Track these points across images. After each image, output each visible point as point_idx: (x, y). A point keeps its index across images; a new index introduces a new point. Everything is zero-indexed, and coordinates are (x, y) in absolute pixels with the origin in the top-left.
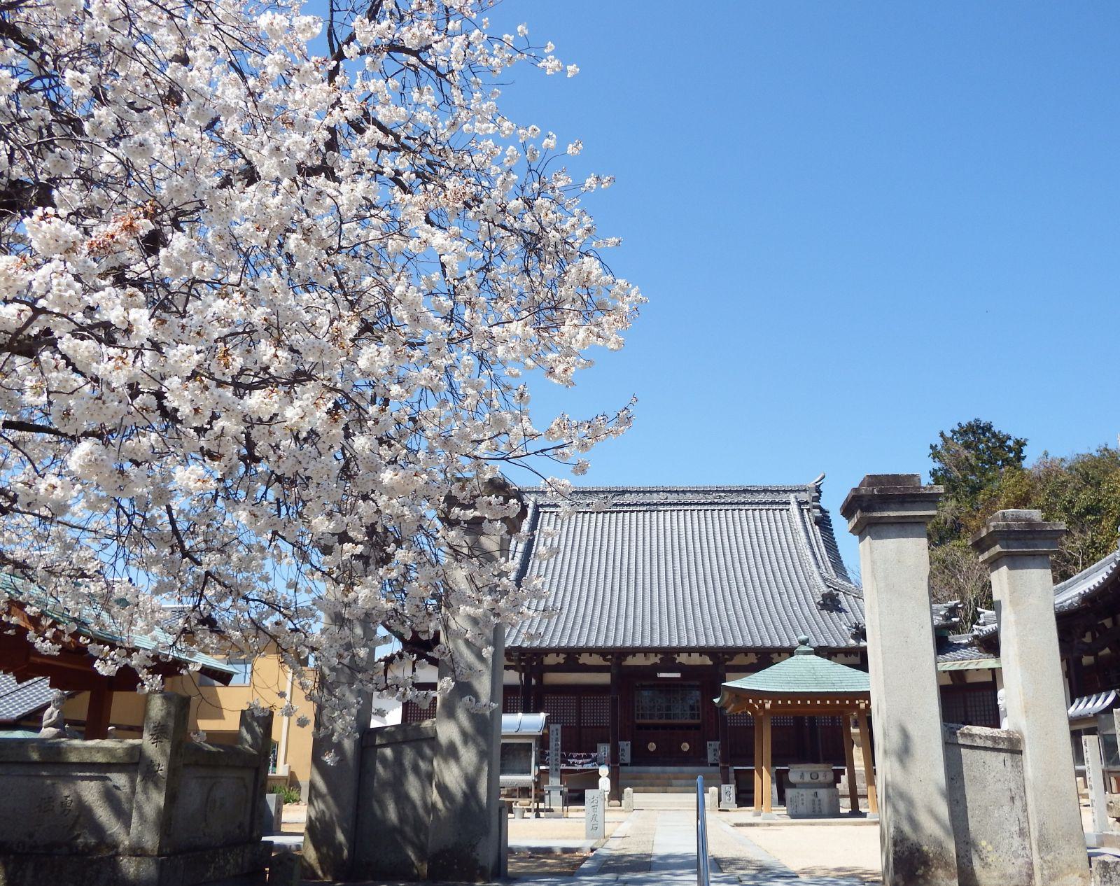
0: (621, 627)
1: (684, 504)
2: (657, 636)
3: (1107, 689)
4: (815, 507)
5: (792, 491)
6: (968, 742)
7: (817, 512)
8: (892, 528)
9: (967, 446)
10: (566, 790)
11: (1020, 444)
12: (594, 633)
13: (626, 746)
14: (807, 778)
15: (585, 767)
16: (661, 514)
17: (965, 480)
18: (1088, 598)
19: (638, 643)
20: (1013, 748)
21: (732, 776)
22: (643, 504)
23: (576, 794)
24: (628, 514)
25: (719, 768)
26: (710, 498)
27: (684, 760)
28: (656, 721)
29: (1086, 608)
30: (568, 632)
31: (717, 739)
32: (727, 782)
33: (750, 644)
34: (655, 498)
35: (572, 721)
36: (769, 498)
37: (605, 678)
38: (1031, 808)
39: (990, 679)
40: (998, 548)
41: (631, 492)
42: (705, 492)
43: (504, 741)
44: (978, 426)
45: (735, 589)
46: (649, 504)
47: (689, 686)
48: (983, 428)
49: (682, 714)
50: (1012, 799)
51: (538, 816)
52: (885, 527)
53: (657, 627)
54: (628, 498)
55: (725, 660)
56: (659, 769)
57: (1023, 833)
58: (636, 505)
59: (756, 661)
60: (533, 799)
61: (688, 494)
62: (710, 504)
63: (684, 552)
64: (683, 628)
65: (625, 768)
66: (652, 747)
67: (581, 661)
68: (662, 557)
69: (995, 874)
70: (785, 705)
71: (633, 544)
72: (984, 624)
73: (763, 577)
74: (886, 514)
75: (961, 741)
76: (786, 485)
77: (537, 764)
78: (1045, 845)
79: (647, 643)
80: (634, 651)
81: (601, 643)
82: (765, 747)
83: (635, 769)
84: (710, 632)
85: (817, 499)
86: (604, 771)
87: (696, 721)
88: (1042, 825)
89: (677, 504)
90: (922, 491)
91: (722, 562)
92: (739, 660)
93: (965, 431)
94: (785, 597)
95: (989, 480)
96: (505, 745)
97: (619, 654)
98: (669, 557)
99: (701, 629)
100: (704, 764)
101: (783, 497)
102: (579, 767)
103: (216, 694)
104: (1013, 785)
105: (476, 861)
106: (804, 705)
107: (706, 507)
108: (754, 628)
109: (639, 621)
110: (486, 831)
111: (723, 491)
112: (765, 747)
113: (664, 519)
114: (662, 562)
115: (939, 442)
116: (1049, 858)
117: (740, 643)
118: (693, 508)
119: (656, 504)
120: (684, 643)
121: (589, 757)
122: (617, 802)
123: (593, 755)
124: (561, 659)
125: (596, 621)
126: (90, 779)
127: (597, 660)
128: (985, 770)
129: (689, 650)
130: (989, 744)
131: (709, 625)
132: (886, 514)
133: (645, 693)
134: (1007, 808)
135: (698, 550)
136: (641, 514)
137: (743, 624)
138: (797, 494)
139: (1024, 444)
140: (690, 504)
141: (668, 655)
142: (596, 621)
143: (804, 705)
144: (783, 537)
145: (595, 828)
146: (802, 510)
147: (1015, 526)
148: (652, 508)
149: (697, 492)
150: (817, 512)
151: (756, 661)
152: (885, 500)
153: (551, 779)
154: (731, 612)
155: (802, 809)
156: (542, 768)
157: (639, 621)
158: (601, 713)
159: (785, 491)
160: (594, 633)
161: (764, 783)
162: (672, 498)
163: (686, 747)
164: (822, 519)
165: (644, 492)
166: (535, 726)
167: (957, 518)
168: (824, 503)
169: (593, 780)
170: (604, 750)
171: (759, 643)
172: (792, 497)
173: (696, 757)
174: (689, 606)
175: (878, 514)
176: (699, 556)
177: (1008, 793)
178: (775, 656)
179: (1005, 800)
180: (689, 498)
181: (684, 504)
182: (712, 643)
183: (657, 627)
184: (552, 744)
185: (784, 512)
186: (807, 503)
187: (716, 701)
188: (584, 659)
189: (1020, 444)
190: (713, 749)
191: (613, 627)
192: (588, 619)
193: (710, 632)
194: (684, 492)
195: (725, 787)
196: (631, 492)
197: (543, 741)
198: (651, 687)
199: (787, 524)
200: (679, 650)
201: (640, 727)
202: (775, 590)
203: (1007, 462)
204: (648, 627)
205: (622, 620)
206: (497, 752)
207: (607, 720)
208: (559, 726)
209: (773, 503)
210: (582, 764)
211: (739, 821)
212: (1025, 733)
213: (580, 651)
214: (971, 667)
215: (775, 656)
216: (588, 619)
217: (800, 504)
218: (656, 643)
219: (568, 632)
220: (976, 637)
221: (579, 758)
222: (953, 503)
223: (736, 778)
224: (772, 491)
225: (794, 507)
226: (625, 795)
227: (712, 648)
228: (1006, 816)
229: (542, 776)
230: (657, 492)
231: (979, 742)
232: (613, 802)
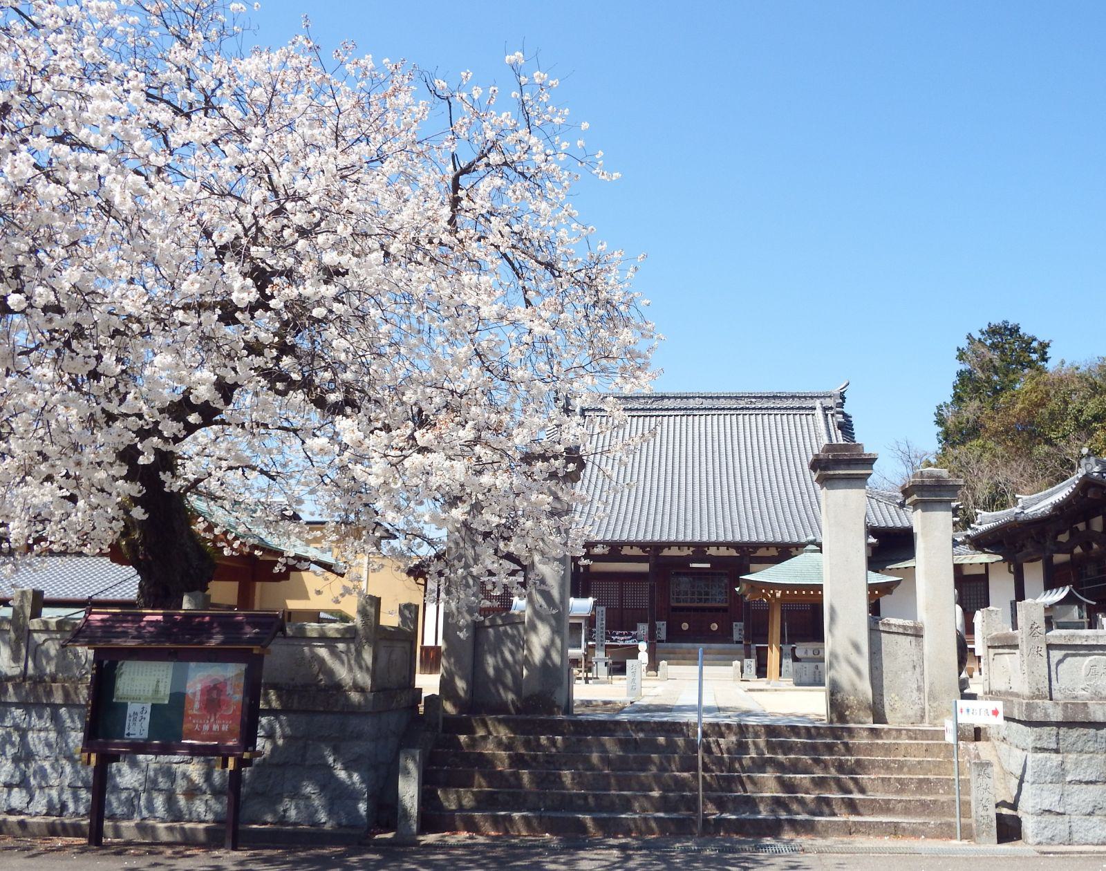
0: (659, 523)
1: (717, 409)
2: (689, 532)
3: (1064, 585)
4: (838, 413)
5: (818, 397)
7: (840, 418)
8: (842, 483)
9: (994, 347)
10: (611, 661)
11: (1044, 346)
12: (635, 529)
13: (662, 626)
14: (810, 654)
15: (627, 643)
17: (988, 380)
18: (1057, 507)
19: (673, 538)
20: (917, 633)
21: (754, 652)
22: (680, 409)
24: (666, 418)
26: (742, 404)
28: (682, 604)
30: (611, 527)
32: (749, 656)
33: (771, 539)
36: (796, 403)
37: (644, 567)
38: (926, 673)
40: (915, 497)
41: (669, 398)
42: (737, 398)
45: (761, 489)
46: (686, 409)
47: (719, 574)
48: (1010, 330)
50: (914, 667)
52: (836, 481)
53: (690, 523)
54: (667, 403)
56: (690, 645)
57: (919, 689)
60: (583, 669)
61: (722, 400)
62: (742, 409)
66: (685, 626)
67: (623, 553)
68: (697, 459)
70: (792, 594)
71: (671, 446)
73: (787, 478)
74: (837, 472)
75: (881, 628)
77: (586, 641)
78: (933, 697)
79: (681, 538)
80: (669, 545)
81: (640, 538)
82: (775, 630)
83: (670, 645)
85: (841, 405)
86: (643, 646)
87: (724, 605)
88: (932, 684)
89: (711, 409)
90: (863, 457)
92: (761, 552)
95: (1011, 381)
97: (658, 547)
98: (703, 458)
101: (809, 403)
102: (622, 643)
104: (915, 658)
106: (808, 594)
107: (738, 412)
108: (775, 524)
110: (560, 684)
111: (755, 397)
112: (775, 630)
113: (699, 423)
114: (697, 464)
115: (964, 344)
117: (762, 539)
118: (726, 412)
120: (713, 539)
121: (630, 634)
122: (654, 673)
123: (633, 633)
124: (606, 550)
125: (636, 517)
127: (637, 551)
128: (896, 649)
129: (718, 545)
130: (901, 630)
132: (837, 472)
136: (678, 418)
137: (767, 521)
138: (822, 400)
139: (1048, 345)
140: (724, 409)
141: (700, 549)
142: (636, 517)
143: (808, 594)
145: (632, 688)
146: (827, 415)
147: (927, 481)
148: (689, 412)
150: (840, 418)
152: (837, 463)
153: (596, 653)
154: (757, 510)
155: (805, 679)
156: (590, 643)
158: (641, 597)
159: (812, 398)
160: (635, 529)
161: (773, 656)
165: (682, 398)
166: (585, 609)
167: (978, 418)
169: (634, 653)
170: (643, 629)
171: (779, 539)
172: (817, 403)
173: (724, 636)
175: (831, 472)
177: (911, 663)
178: (793, 550)
180: (722, 403)
181: (717, 409)
182: (738, 538)
183: (690, 523)
184: (598, 623)
185: (810, 417)
186: (831, 408)
187: (737, 589)
188: (626, 551)
189: (1044, 346)
190: (738, 629)
192: (629, 516)
194: (718, 398)
195: (747, 661)
196: (669, 398)
197: (591, 621)
198: (685, 574)
199: (812, 428)
200: (709, 545)
201: (675, 609)
202: (797, 490)
203: (1031, 364)
204: (682, 523)
205: (659, 517)
206: (566, 631)
207: (646, 602)
208: (604, 608)
210: (624, 640)
213: (622, 544)
215: (793, 550)
216: (629, 516)
217: (825, 409)
218: (689, 539)
219: (611, 527)
220: (968, 536)
221: (621, 635)
222: (976, 403)
223: (758, 654)
224: (799, 398)
225: (819, 413)
227: (738, 543)
228: (910, 679)
229: (590, 650)
231: (894, 629)
232: (650, 673)
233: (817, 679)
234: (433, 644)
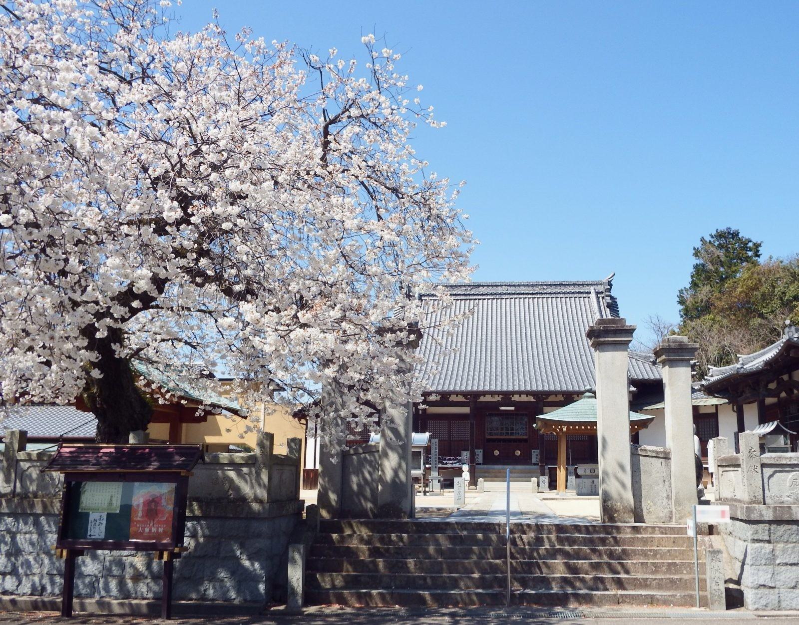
1: (519, 294)
2: (499, 383)
3: (773, 421)
4: (607, 296)
5: (592, 285)
6: (644, 454)
7: (608, 300)
8: (610, 347)
9: (720, 247)
10: (442, 479)
11: (757, 246)
12: (459, 382)
13: (479, 453)
14: (588, 472)
15: (454, 465)
16: (503, 301)
18: (768, 363)
19: (487, 389)
20: (666, 457)
21: (547, 471)
22: (491, 294)
23: (448, 482)
25: (538, 467)
26: (537, 290)
27: (516, 461)
29: (767, 370)
30: (442, 381)
31: (537, 448)
32: (543, 474)
33: (558, 389)
34: (500, 290)
35: (446, 437)
36: (577, 289)
37: (466, 410)
39: (714, 411)
40: (664, 357)
41: (483, 286)
43: (413, 450)
44: (729, 233)
46: (496, 294)
48: (732, 234)
49: (521, 433)
50: (664, 481)
51: (425, 494)
53: (499, 377)
54: (482, 290)
55: (544, 400)
58: (487, 294)
59: (563, 399)
60: (422, 485)
61: (522, 287)
63: (518, 327)
64: (516, 378)
65: (479, 466)
67: (450, 400)
69: (653, 516)
71: (485, 322)
72: (712, 376)
74: (606, 339)
75: (640, 453)
76: (588, 280)
77: (424, 464)
78: (678, 503)
79: (493, 388)
80: (484, 393)
81: (463, 389)
83: (485, 466)
84: (534, 381)
85: (609, 290)
86: (466, 468)
87: (525, 437)
88: (677, 493)
89: (514, 294)
90: (625, 328)
91: (543, 333)
92: (551, 398)
93: (720, 235)
94: (584, 358)
95: (733, 272)
96: (413, 452)
97: (476, 395)
99: (528, 379)
100: (530, 464)
101: (586, 289)
102: (450, 466)
103: (216, 419)
104: (665, 474)
105: (401, 509)
107: (534, 296)
108: (562, 378)
109: (488, 374)
110: (406, 496)
111: (546, 285)
113: (505, 304)
115: (698, 245)
116: (679, 509)
117: (552, 388)
118: (525, 296)
119: (500, 294)
120: (517, 389)
121: (456, 459)
122: (474, 487)
123: (458, 458)
125: (460, 374)
126: (230, 470)
127: (461, 398)
128: (651, 468)
129: (520, 393)
130: (654, 454)
131: (533, 376)
132: (606, 339)
133: (496, 418)
134: (661, 485)
135: (528, 325)
138: (595, 286)
139: (760, 245)
140: (523, 294)
141: (507, 396)
142: (460, 374)
144: (585, 316)
145: (459, 499)
146: (599, 298)
147: (673, 345)
148: (498, 297)
149: (528, 285)
150: (608, 300)
151: (563, 399)
152: (607, 332)
155: (584, 490)
156: (427, 466)
157: (488, 374)
158: (464, 432)
159: (587, 285)
160: (459, 382)
161: (561, 474)
162: (511, 290)
163: (518, 453)
164: (612, 304)
165: (492, 286)
167: (709, 298)
168: (613, 293)
169: (459, 472)
170: (466, 455)
171: (564, 389)
172: (592, 289)
173: (525, 460)
174: (521, 364)
176: (528, 330)
178: (575, 396)
179: (661, 481)
181: (519, 294)
182: (535, 388)
183: (499, 377)
184: (433, 451)
186: (602, 293)
187: (534, 425)
188: (453, 398)
189: (757, 246)
190: (535, 454)
191: (471, 378)
192: (455, 373)
193: (534, 381)
194: (519, 286)
195: (542, 478)
196: (483, 286)
197: (428, 450)
198: (496, 415)
199: (588, 307)
200: (513, 393)
201: (489, 440)
203: (748, 259)
207: (467, 436)
208: (437, 440)
209: (579, 293)
210: (452, 464)
211: (545, 497)
212: (672, 450)
213: (450, 393)
214: (701, 404)
215: (575, 396)
216: (455, 373)
217: (597, 293)
218: (499, 389)
220: (702, 385)
221: (450, 460)
222: (708, 288)
224: (579, 285)
225: (593, 296)
226: (479, 483)
230: (501, 286)
231: (649, 454)
232: (471, 487)
233: (594, 491)
234: (312, 468)
